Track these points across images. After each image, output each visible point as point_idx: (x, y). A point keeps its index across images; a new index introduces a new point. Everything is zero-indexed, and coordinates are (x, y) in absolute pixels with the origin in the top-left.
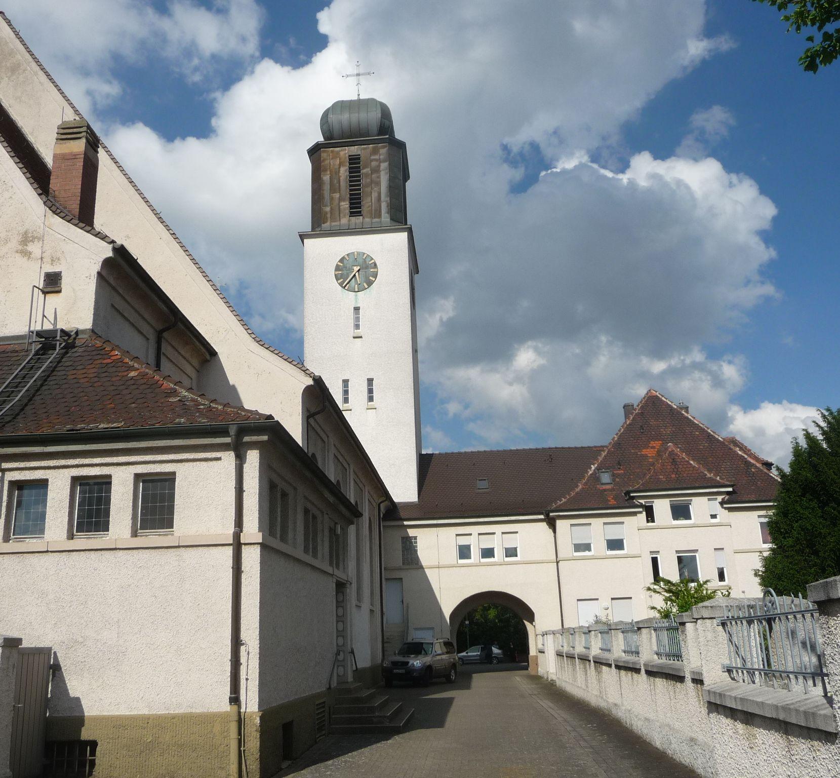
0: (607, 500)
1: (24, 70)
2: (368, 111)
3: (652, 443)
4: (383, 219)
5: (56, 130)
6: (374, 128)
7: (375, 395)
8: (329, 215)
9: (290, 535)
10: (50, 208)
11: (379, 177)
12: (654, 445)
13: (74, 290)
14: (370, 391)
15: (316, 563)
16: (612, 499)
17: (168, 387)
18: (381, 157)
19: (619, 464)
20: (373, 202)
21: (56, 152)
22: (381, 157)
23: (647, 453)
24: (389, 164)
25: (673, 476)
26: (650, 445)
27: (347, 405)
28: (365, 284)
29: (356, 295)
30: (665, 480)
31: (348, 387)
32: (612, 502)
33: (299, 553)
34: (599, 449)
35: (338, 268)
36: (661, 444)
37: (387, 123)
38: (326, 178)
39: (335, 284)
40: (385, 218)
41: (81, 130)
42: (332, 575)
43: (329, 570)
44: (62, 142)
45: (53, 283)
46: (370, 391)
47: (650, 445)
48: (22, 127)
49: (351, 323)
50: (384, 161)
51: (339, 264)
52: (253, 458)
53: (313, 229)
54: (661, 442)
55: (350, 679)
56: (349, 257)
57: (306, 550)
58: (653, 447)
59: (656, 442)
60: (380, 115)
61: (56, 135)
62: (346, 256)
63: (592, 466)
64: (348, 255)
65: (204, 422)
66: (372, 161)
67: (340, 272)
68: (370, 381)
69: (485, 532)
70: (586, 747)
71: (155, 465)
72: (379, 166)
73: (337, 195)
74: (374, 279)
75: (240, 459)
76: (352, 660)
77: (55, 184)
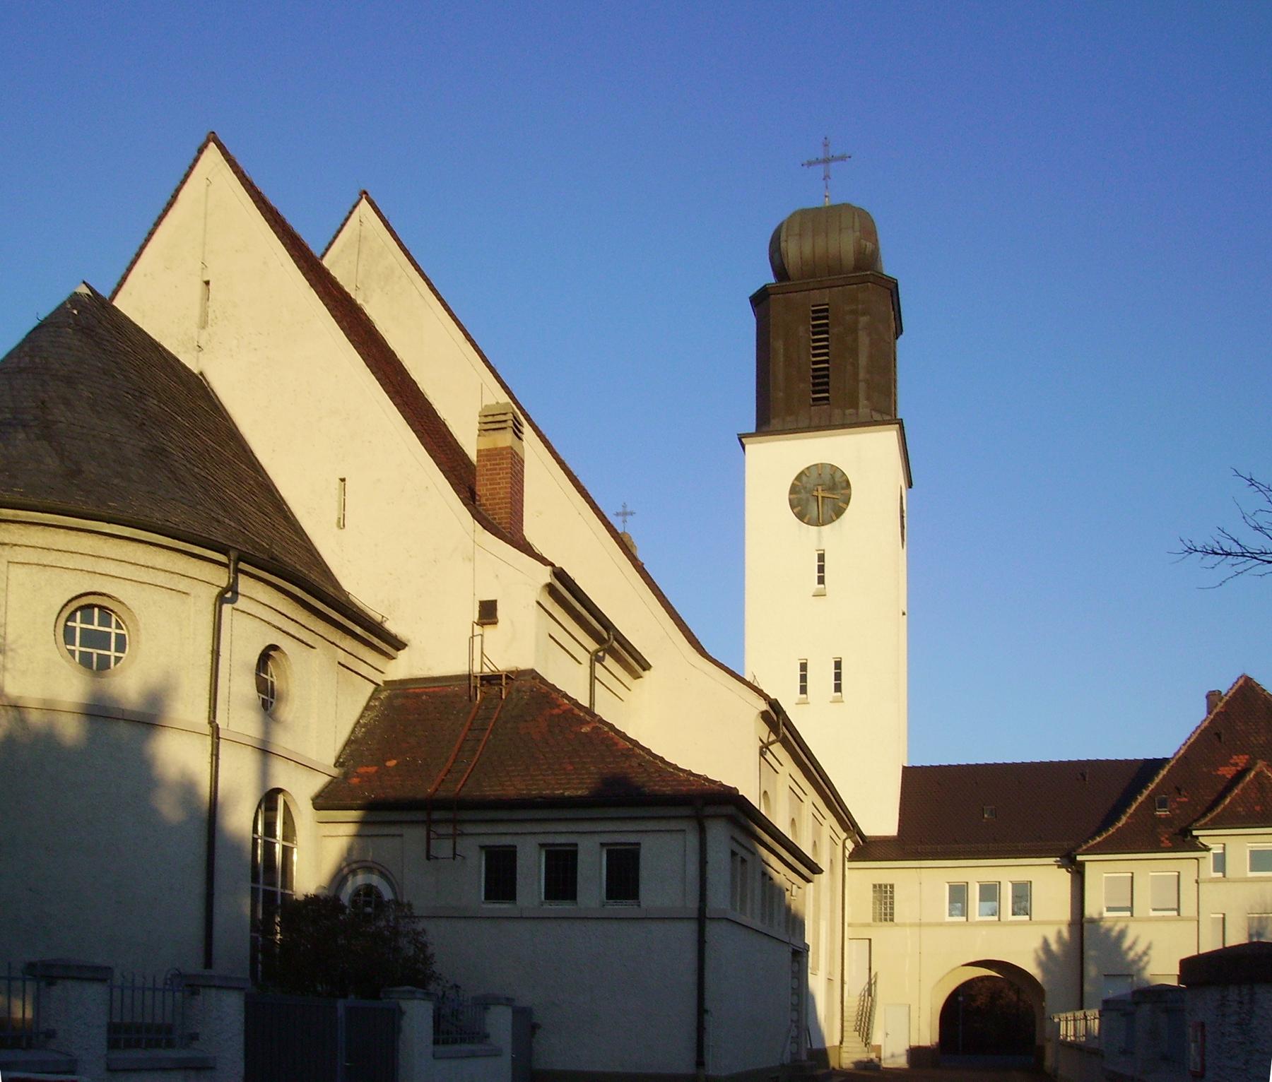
4: (861, 410)
9: (749, 905)
11: (856, 340)
15: (745, 920)
16: (1167, 839)
17: (626, 746)
19: (1178, 790)
21: (479, 448)
23: (1225, 773)
25: (1258, 808)
26: (1232, 761)
29: (820, 532)
32: (1167, 844)
33: (757, 924)
34: (1166, 760)
35: (793, 490)
36: (1246, 759)
44: (486, 433)
45: (488, 612)
47: (1232, 761)
48: (402, 359)
51: (796, 482)
55: (804, 1057)
56: (810, 473)
57: (762, 920)
59: (1241, 757)
61: (478, 424)
63: (1139, 797)
64: (808, 468)
69: (840, 950)
70: (146, 431)
76: (806, 1038)
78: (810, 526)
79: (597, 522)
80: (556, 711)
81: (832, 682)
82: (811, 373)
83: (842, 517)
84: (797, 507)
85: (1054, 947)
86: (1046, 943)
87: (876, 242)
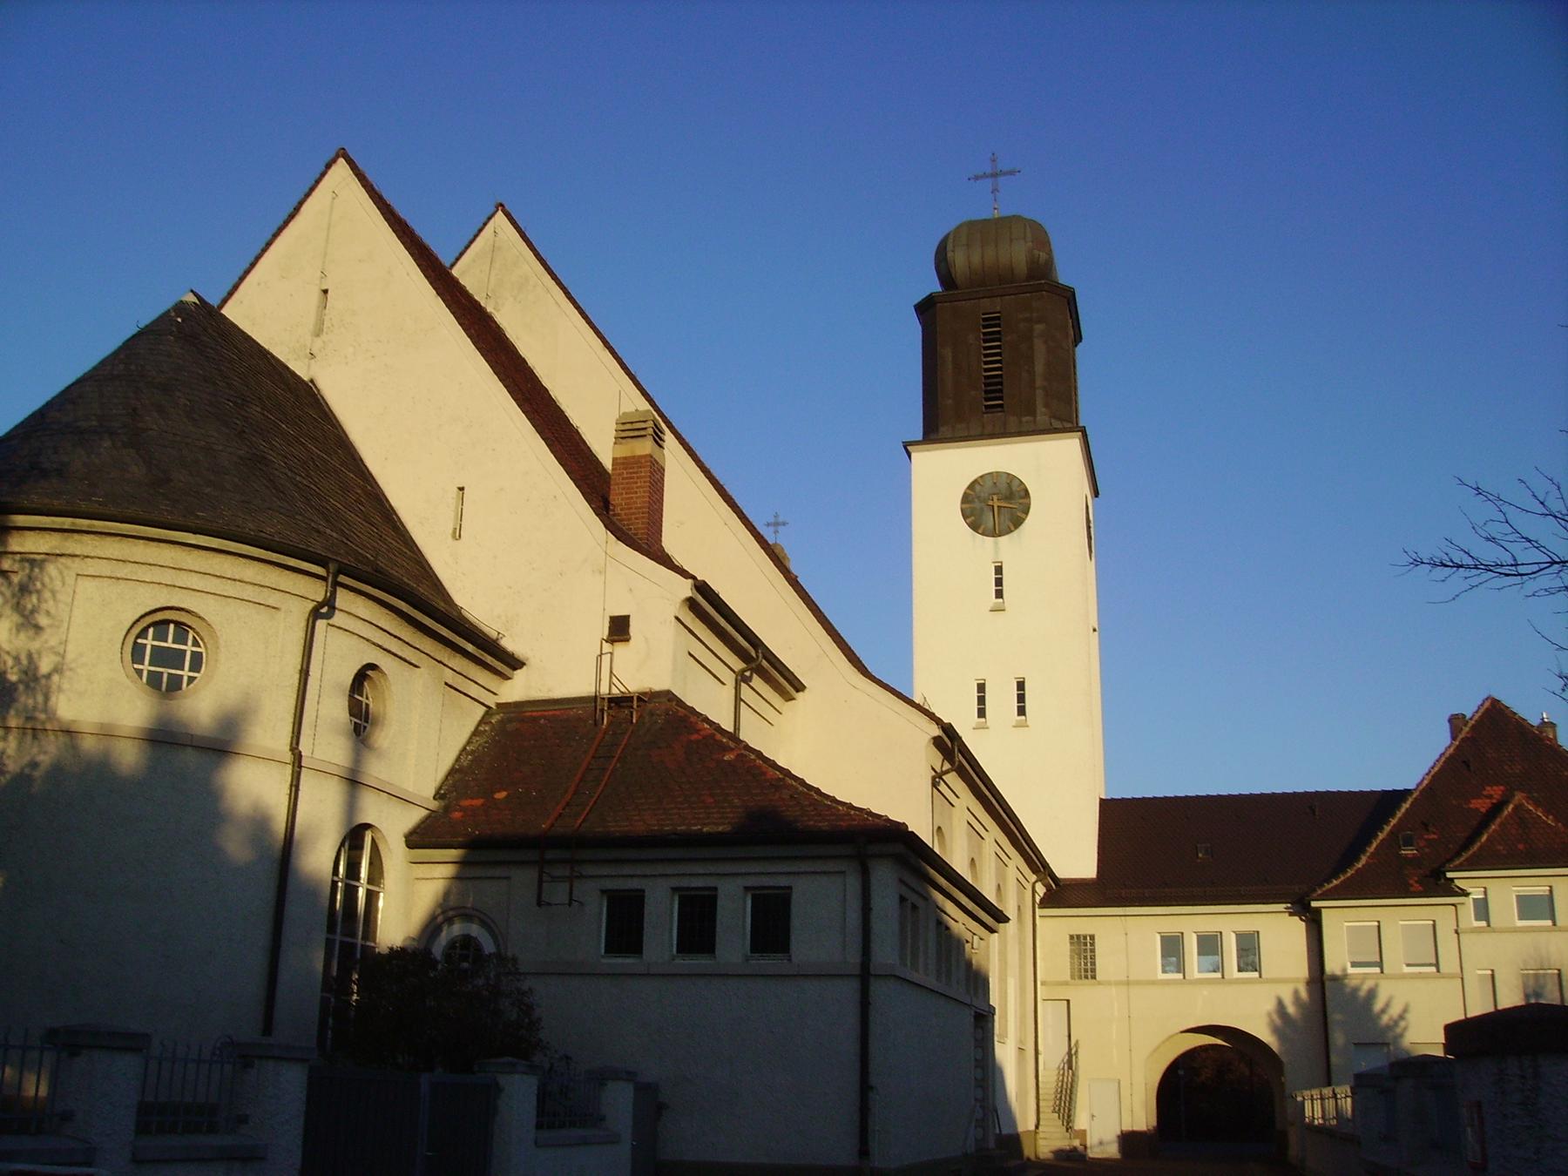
0: (1409, 884)
3: (1489, 790)
4: (1038, 418)
5: (615, 426)
12: (1492, 793)
13: (646, 639)
16: (1416, 882)
21: (615, 456)
22: (1035, 315)
23: (1478, 806)
25: (1521, 846)
26: (1485, 793)
29: (996, 543)
30: (1505, 852)
32: (1417, 887)
33: (931, 982)
37: (1043, 256)
41: (643, 425)
42: (969, 1006)
43: (968, 1001)
44: (624, 441)
45: (619, 629)
47: (1485, 793)
51: (968, 491)
53: (926, 433)
54: (1502, 788)
55: (992, 1145)
58: (1490, 797)
59: (1495, 788)
63: (1379, 834)
76: (994, 1121)
77: (616, 499)
78: (985, 537)
82: (1002, 324)
83: (1021, 527)
84: (972, 515)
87: (1050, 253)
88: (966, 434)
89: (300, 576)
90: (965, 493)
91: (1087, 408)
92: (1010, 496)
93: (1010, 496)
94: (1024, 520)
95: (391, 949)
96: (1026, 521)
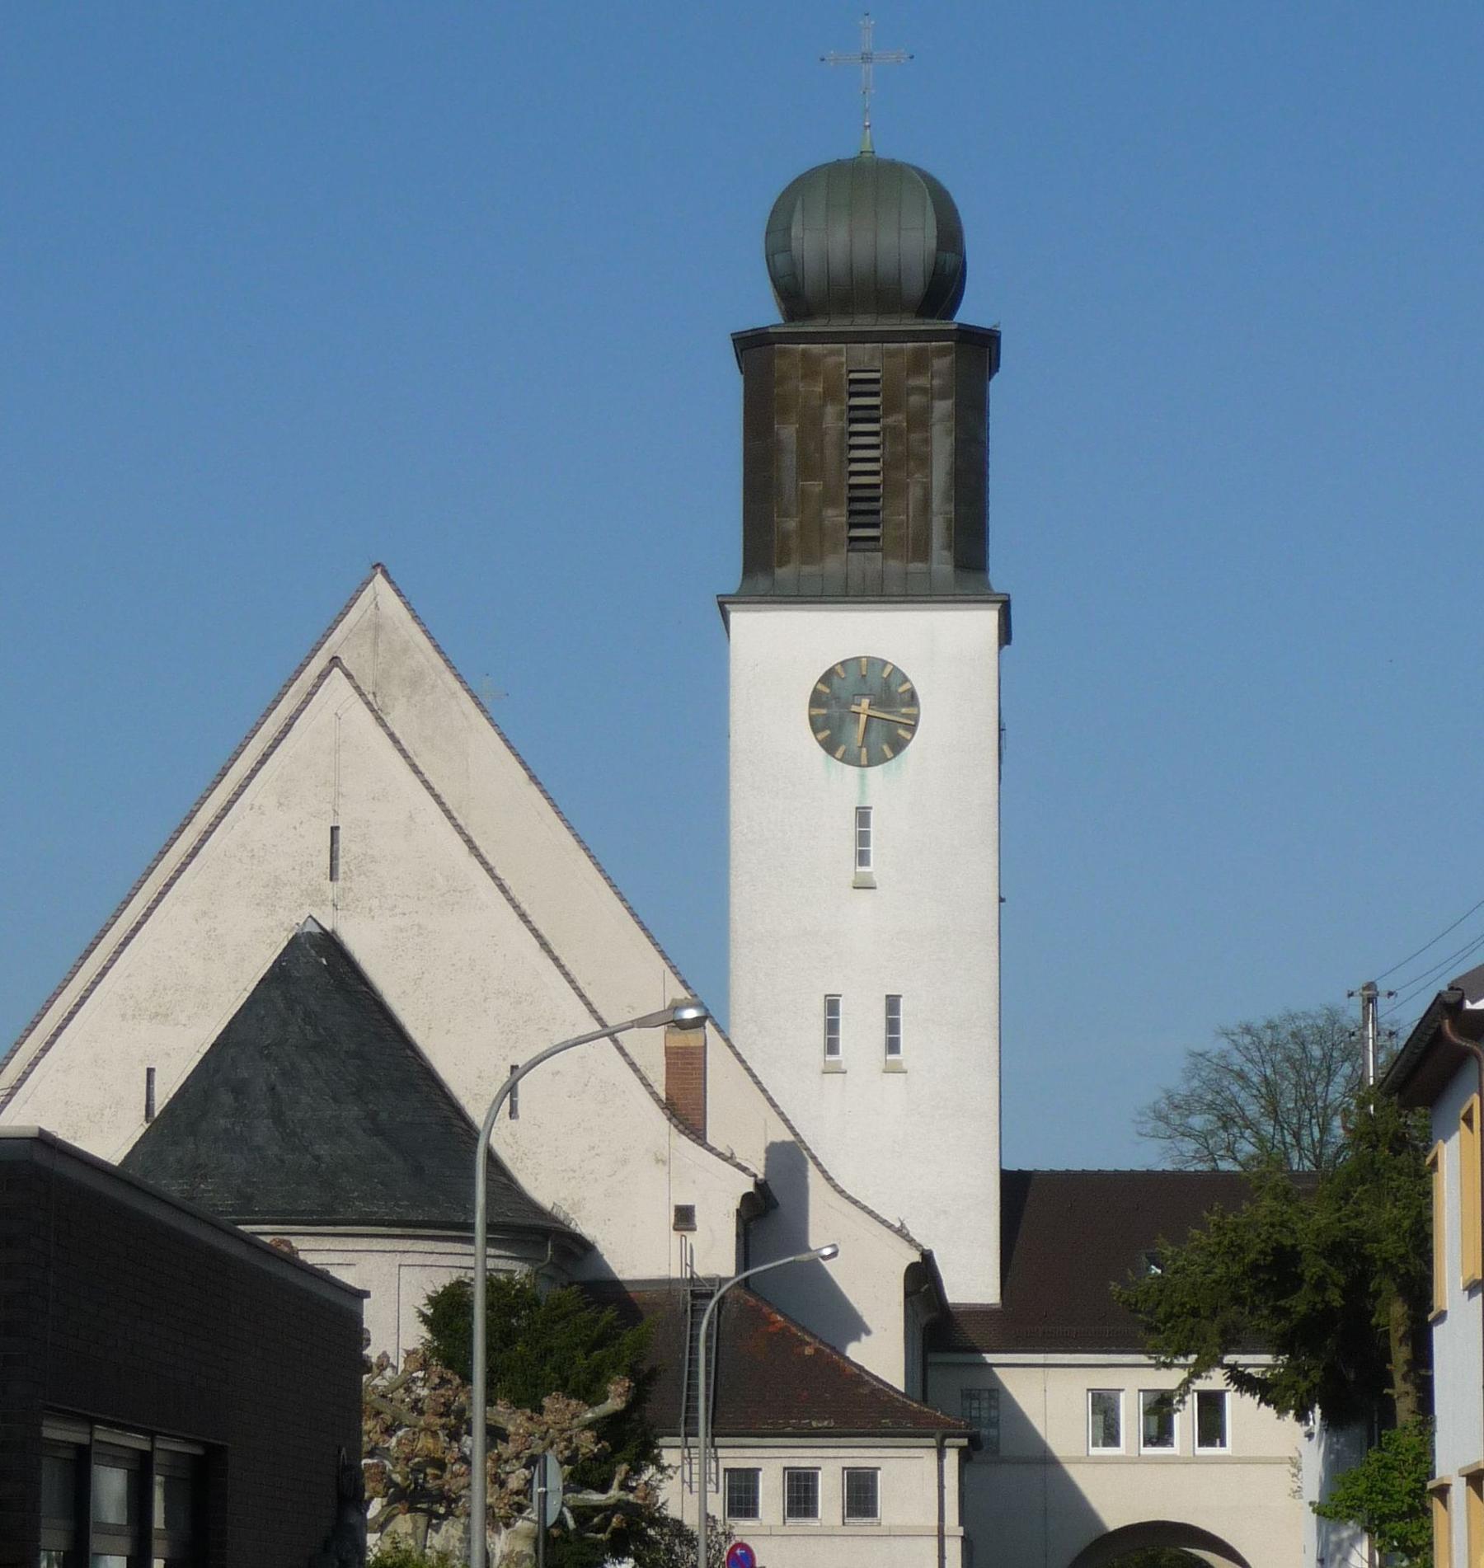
1: (433, 687)
2: (900, 229)
4: (935, 566)
6: (915, 285)
7: (903, 1036)
8: (794, 543)
10: (676, 1126)
11: (927, 441)
14: (893, 1026)
18: (936, 382)
20: (911, 514)
22: (936, 382)
24: (957, 405)
27: (833, 1058)
28: (886, 748)
29: (862, 777)
31: (838, 1014)
35: (816, 700)
38: (788, 432)
39: (808, 744)
40: (941, 562)
45: (684, 1218)
46: (893, 1026)
49: (850, 848)
50: (943, 396)
51: (820, 687)
52: (952, 1458)
56: (845, 671)
60: (932, 244)
62: (839, 669)
64: (843, 663)
65: (910, 1428)
66: (912, 391)
67: (824, 711)
68: (893, 1003)
71: (860, 1456)
72: (927, 410)
73: (816, 486)
74: (909, 737)
75: (941, 1457)
78: (845, 765)
79: (858, 1303)
80: (771, 1329)
81: (880, 1035)
82: (846, 491)
83: (903, 753)
84: (823, 729)
85: (429, 1312)
86: (422, 1314)
87: (961, 255)
88: (885, 345)
89: (326, 1238)
90: (815, 691)
91: (999, 576)
92: (588, 1391)
93: (588, 1391)
94: (908, 741)
95: (1342, 1429)
96: (911, 744)
